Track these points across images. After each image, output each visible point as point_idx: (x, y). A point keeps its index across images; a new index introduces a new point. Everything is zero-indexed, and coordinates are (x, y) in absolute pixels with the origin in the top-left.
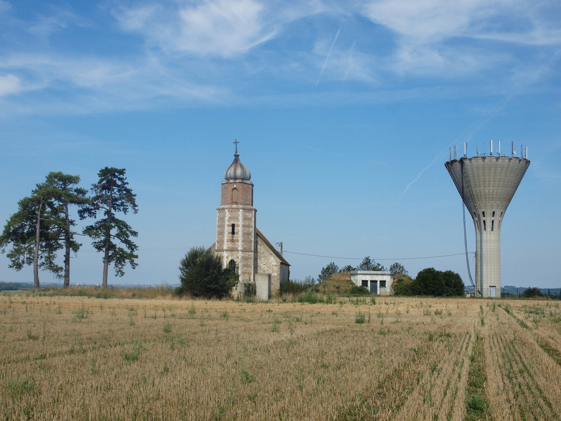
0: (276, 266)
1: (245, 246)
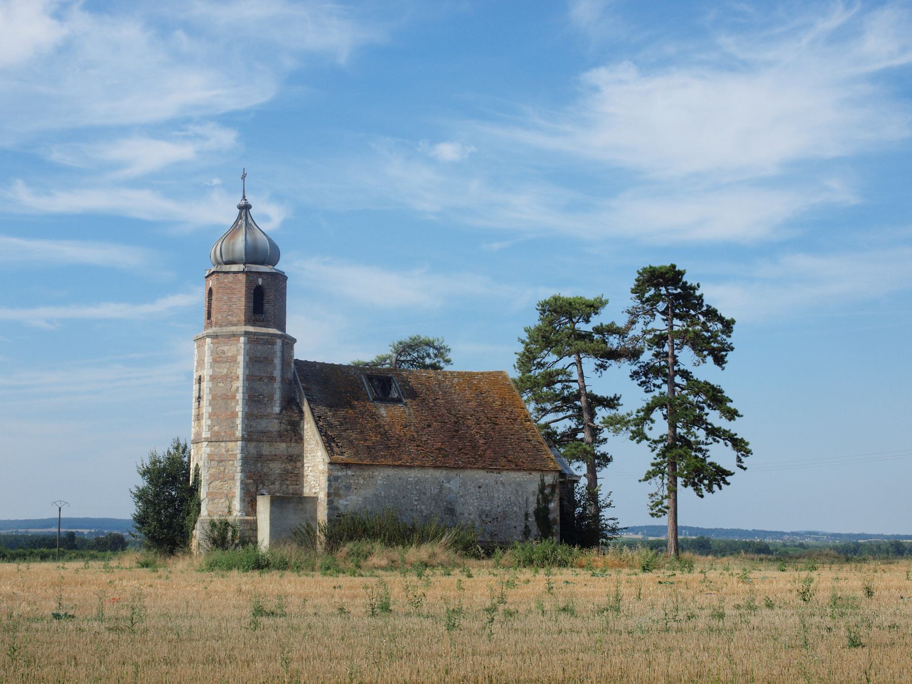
1: (216, 428)
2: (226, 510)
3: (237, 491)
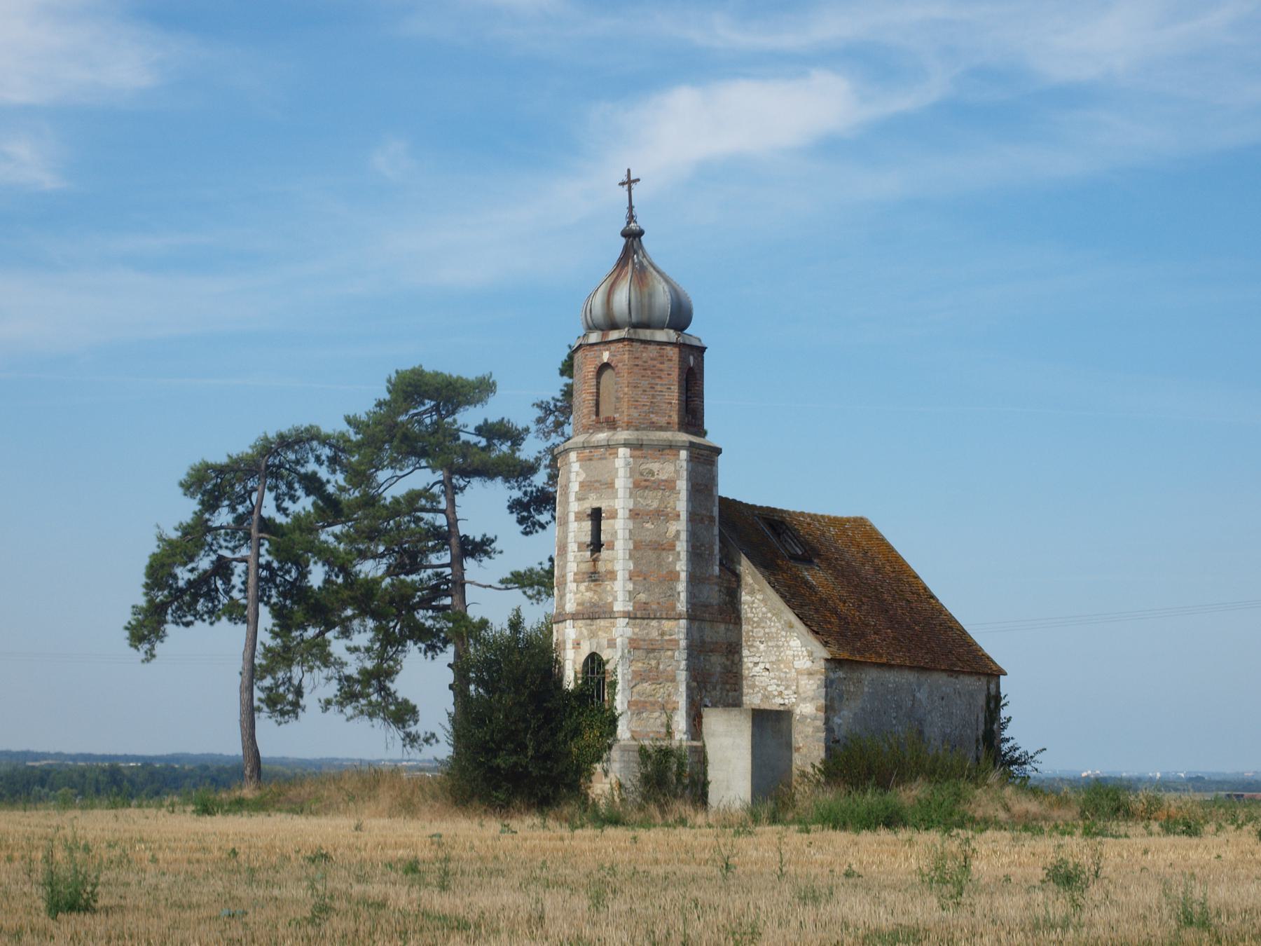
0: (810, 674)
1: (643, 597)
2: (663, 730)
3: (682, 701)
